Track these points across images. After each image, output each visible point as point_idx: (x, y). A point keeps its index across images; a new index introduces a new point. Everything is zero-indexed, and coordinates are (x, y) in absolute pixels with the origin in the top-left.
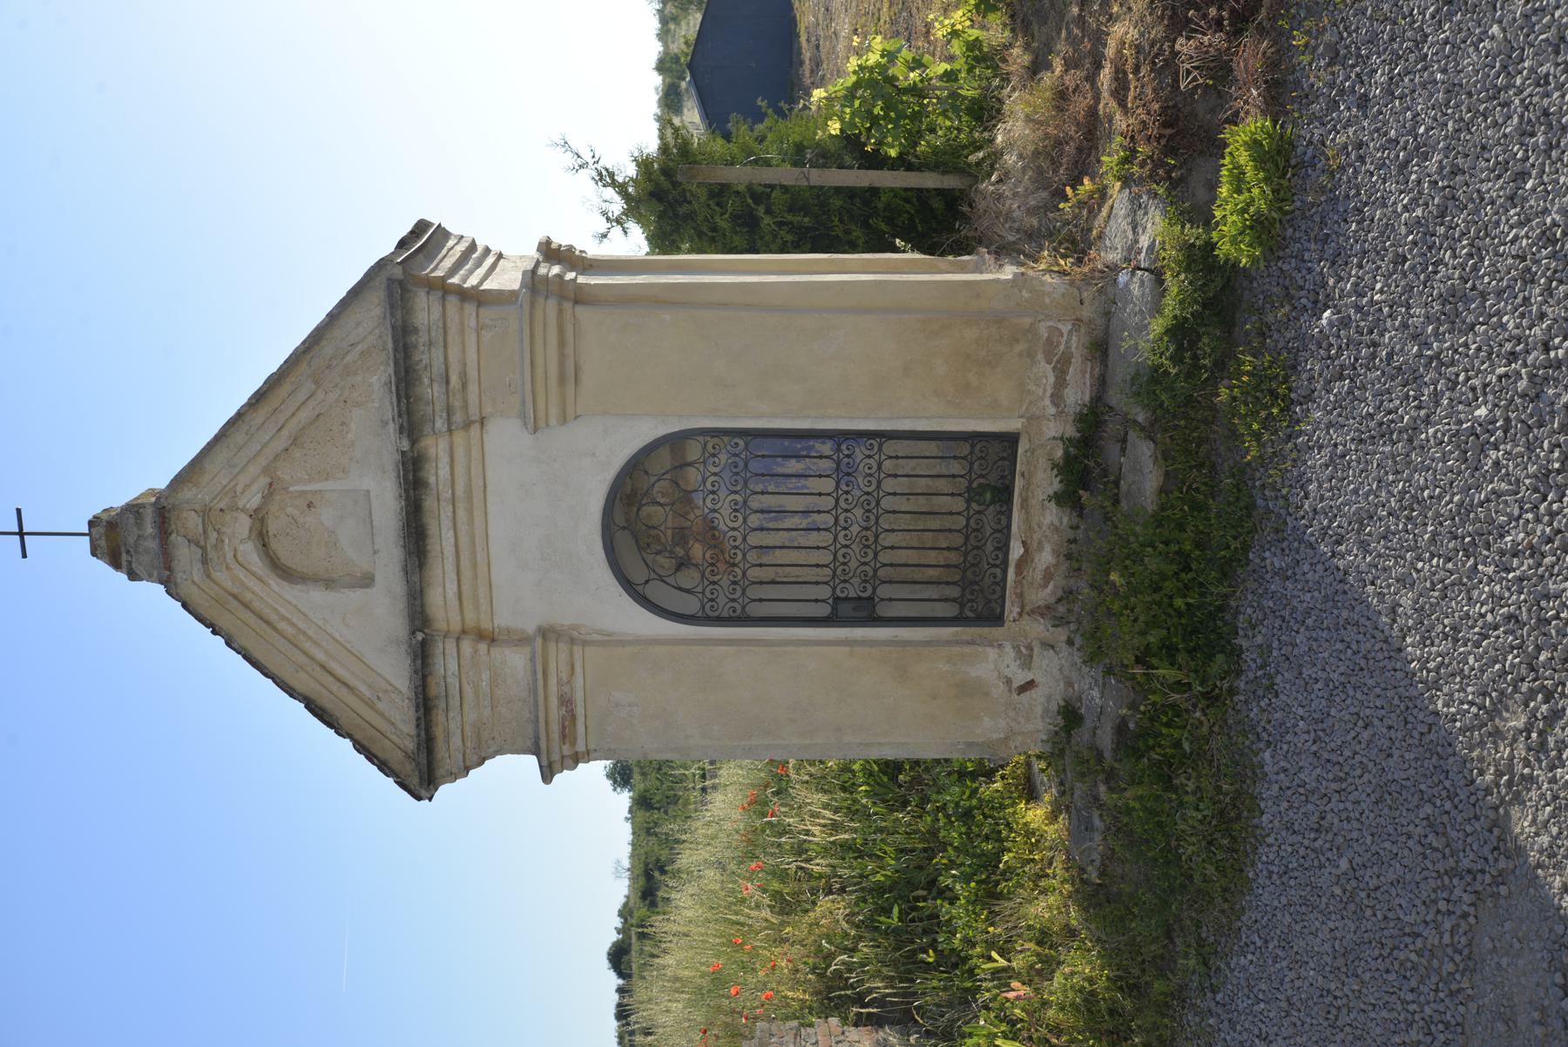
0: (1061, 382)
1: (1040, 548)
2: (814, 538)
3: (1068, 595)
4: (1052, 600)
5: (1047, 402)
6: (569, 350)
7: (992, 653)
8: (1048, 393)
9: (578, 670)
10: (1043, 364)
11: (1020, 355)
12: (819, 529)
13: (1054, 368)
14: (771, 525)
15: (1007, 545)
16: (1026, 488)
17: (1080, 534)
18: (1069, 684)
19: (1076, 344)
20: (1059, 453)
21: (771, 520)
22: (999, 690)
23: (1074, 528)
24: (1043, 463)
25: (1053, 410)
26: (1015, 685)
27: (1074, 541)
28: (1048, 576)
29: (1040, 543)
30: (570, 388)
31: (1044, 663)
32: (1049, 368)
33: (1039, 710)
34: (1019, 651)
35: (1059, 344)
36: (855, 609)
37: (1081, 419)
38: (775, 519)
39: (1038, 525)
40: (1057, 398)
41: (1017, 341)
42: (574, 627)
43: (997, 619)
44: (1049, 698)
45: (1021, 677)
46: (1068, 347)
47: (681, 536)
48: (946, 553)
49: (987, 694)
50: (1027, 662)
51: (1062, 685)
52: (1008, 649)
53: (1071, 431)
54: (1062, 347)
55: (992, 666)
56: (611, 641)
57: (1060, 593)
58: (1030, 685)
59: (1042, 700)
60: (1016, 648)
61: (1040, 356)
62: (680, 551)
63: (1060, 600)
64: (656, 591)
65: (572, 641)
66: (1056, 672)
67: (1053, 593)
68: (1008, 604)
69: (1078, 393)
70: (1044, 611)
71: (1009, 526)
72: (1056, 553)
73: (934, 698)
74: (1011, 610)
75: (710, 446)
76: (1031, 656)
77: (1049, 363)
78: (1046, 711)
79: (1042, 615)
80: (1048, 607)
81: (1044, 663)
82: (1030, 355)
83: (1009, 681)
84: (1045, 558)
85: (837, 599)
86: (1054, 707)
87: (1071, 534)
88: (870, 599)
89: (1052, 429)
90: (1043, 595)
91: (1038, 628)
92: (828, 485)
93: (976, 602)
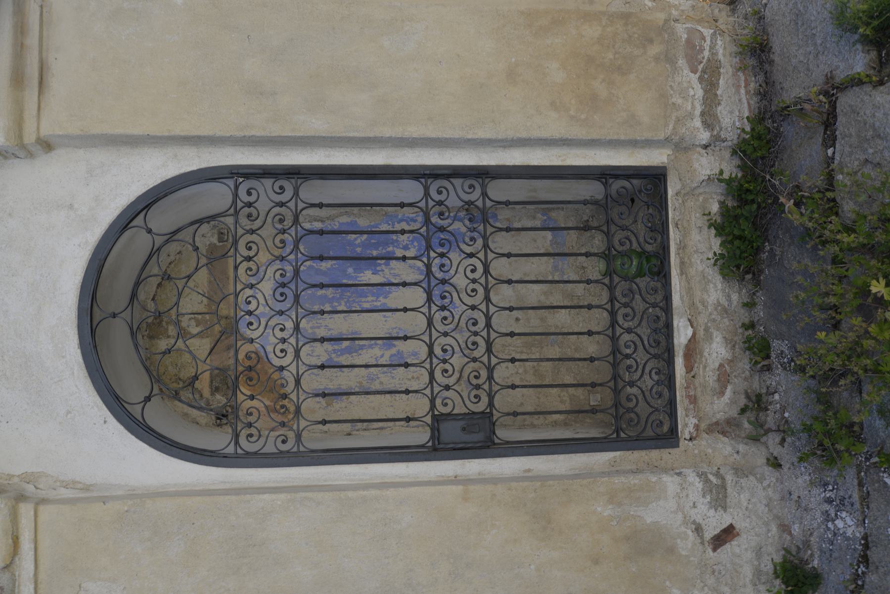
0: (711, 99)
1: (709, 337)
2: (399, 378)
3: (756, 403)
4: (734, 412)
5: (697, 123)
6: (32, 40)
7: (670, 483)
8: (698, 112)
9: (26, 546)
10: (686, 71)
11: (657, 59)
12: (407, 365)
13: (701, 79)
14: (344, 360)
15: (669, 327)
16: (682, 247)
17: (760, 312)
18: (785, 528)
19: (723, 51)
20: (715, 208)
21: (343, 352)
22: (687, 543)
23: (749, 305)
24: (696, 220)
25: (704, 136)
26: (709, 534)
27: (752, 326)
28: (724, 379)
29: (707, 330)
30: (31, 96)
31: (744, 497)
32: (694, 78)
33: (747, 572)
34: (707, 481)
35: (702, 50)
36: (463, 434)
37: (741, 150)
38: (349, 351)
39: (702, 297)
40: (709, 119)
41: (651, 41)
42: (29, 478)
43: (669, 438)
44: (759, 552)
45: (715, 523)
46: (713, 54)
47: (225, 381)
48: (571, 390)
49: (671, 550)
50: (719, 497)
51: (774, 529)
52: (692, 477)
53: (730, 168)
54: (706, 54)
55: (672, 504)
56: (87, 495)
57: (743, 401)
58: (727, 534)
59: (749, 555)
60: (702, 475)
61: (682, 62)
62: (220, 400)
63: (743, 411)
64: (158, 415)
65: (21, 497)
66: (762, 508)
67: (733, 402)
68: (680, 412)
69: (735, 111)
70: (724, 428)
71: (668, 298)
72: (729, 342)
73: (596, 562)
74: (686, 423)
75: (242, 192)
76: (724, 487)
77: (694, 71)
78: (758, 573)
79: (724, 433)
80: (729, 422)
81: (744, 497)
82: (670, 60)
83: (698, 529)
84: (717, 351)
85: (438, 419)
86: (768, 567)
87: (744, 316)
88: (486, 416)
89: (706, 165)
90: (722, 406)
91: (723, 449)
92: (416, 297)
93: (631, 413)
